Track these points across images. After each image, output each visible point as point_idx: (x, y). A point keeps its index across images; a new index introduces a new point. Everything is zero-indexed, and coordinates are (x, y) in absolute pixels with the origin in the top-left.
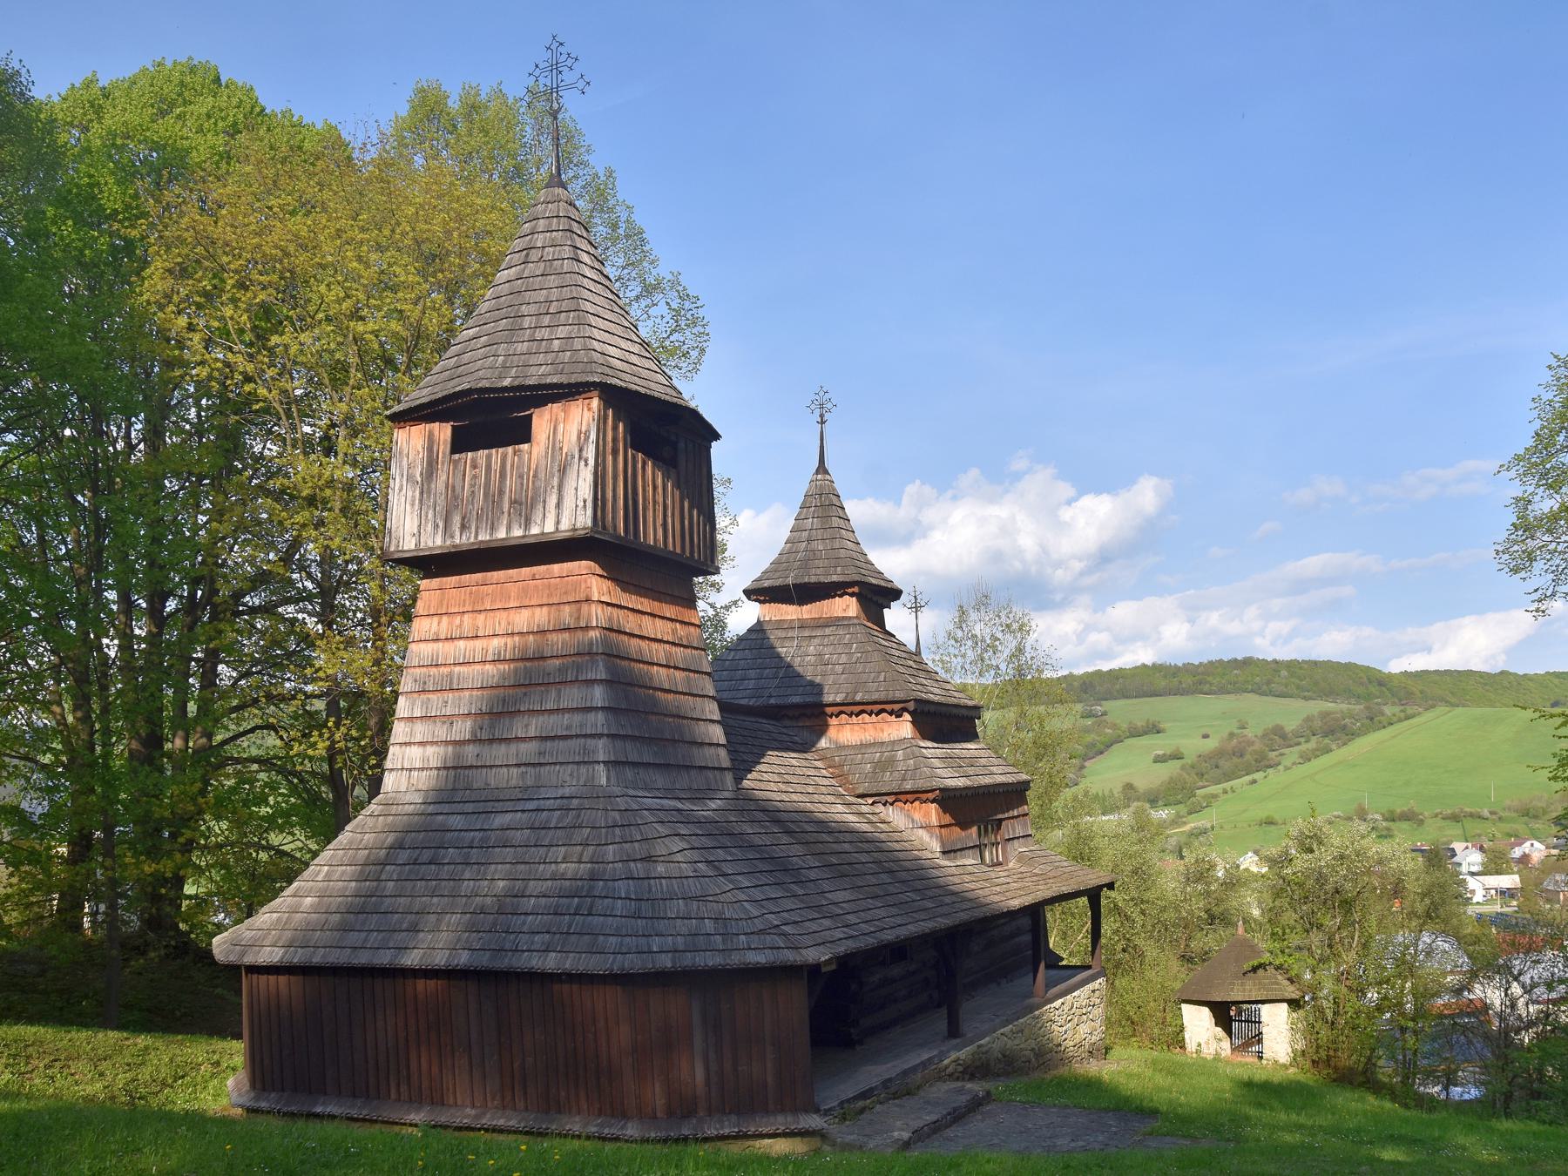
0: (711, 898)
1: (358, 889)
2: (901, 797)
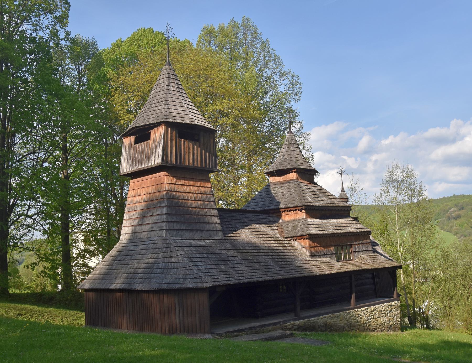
0: (184, 268)
1: (108, 268)
2: (298, 238)
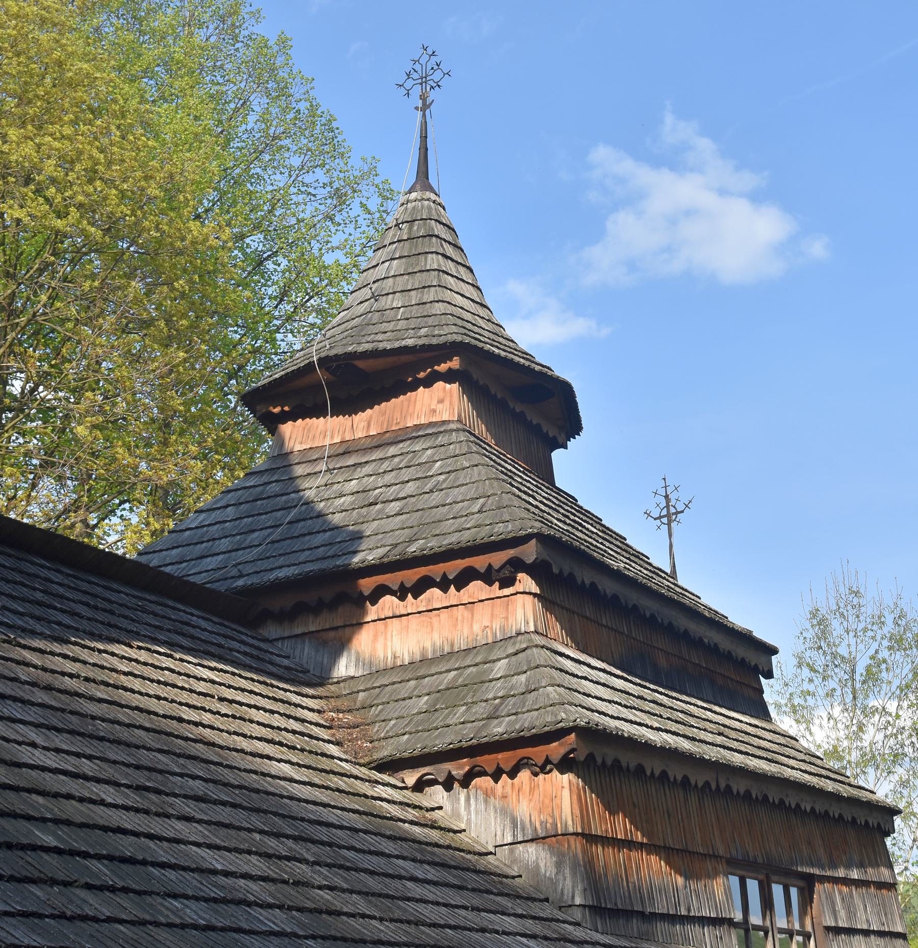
2: (488, 761)
